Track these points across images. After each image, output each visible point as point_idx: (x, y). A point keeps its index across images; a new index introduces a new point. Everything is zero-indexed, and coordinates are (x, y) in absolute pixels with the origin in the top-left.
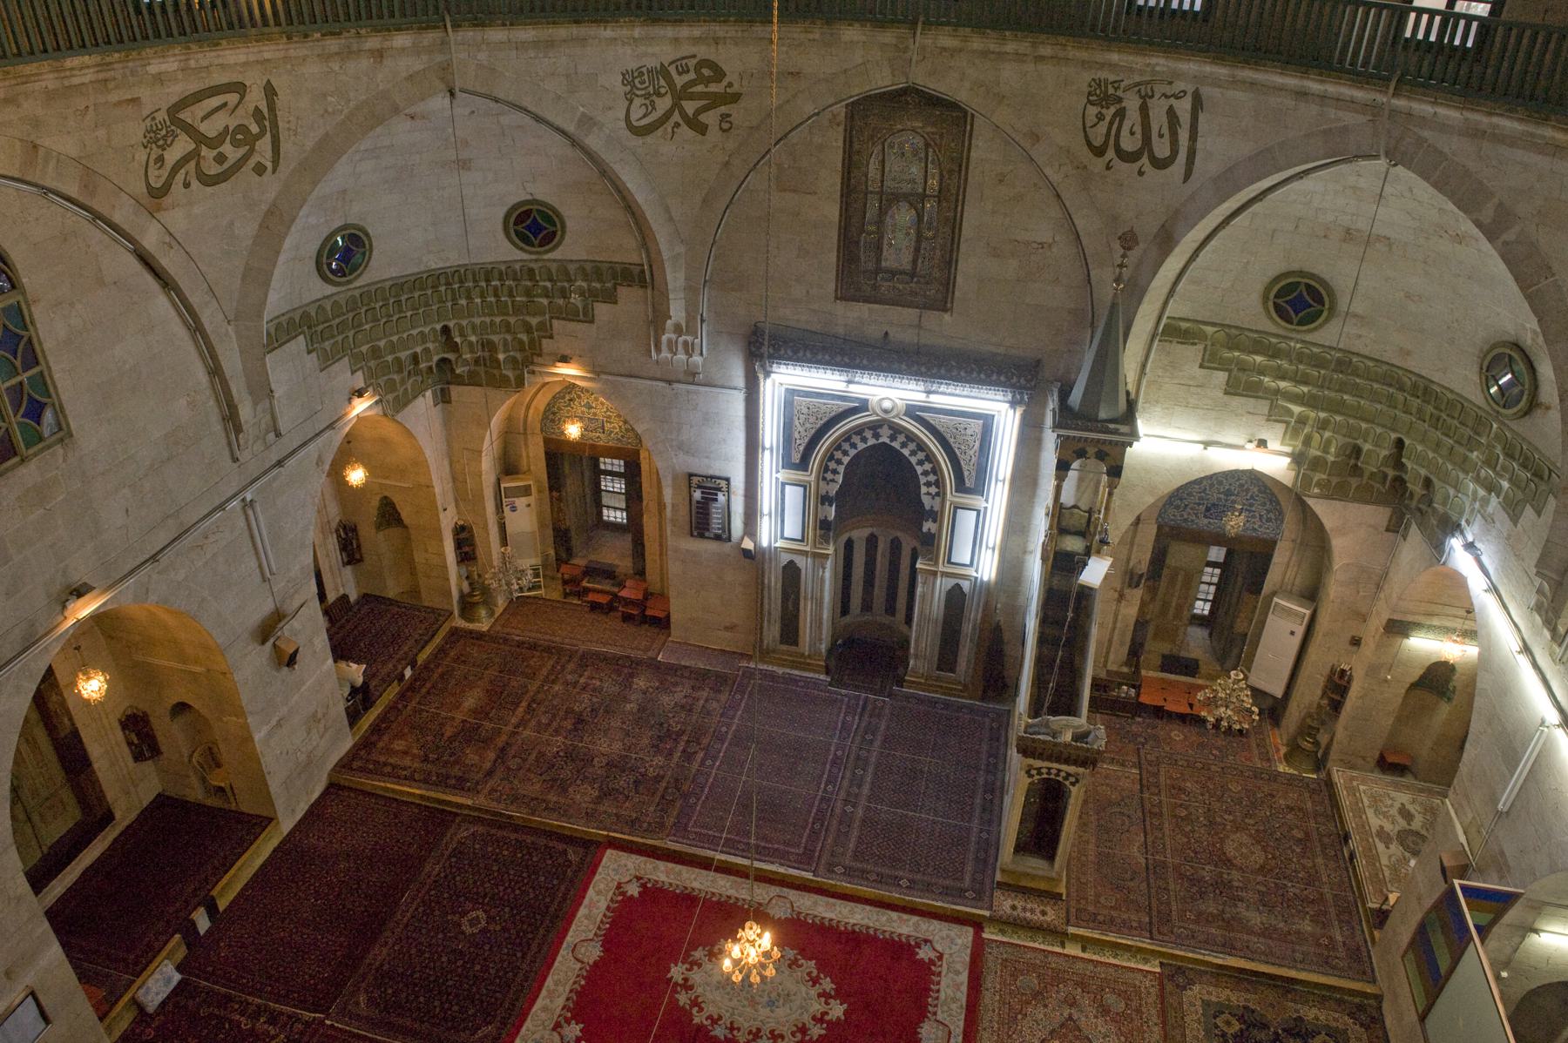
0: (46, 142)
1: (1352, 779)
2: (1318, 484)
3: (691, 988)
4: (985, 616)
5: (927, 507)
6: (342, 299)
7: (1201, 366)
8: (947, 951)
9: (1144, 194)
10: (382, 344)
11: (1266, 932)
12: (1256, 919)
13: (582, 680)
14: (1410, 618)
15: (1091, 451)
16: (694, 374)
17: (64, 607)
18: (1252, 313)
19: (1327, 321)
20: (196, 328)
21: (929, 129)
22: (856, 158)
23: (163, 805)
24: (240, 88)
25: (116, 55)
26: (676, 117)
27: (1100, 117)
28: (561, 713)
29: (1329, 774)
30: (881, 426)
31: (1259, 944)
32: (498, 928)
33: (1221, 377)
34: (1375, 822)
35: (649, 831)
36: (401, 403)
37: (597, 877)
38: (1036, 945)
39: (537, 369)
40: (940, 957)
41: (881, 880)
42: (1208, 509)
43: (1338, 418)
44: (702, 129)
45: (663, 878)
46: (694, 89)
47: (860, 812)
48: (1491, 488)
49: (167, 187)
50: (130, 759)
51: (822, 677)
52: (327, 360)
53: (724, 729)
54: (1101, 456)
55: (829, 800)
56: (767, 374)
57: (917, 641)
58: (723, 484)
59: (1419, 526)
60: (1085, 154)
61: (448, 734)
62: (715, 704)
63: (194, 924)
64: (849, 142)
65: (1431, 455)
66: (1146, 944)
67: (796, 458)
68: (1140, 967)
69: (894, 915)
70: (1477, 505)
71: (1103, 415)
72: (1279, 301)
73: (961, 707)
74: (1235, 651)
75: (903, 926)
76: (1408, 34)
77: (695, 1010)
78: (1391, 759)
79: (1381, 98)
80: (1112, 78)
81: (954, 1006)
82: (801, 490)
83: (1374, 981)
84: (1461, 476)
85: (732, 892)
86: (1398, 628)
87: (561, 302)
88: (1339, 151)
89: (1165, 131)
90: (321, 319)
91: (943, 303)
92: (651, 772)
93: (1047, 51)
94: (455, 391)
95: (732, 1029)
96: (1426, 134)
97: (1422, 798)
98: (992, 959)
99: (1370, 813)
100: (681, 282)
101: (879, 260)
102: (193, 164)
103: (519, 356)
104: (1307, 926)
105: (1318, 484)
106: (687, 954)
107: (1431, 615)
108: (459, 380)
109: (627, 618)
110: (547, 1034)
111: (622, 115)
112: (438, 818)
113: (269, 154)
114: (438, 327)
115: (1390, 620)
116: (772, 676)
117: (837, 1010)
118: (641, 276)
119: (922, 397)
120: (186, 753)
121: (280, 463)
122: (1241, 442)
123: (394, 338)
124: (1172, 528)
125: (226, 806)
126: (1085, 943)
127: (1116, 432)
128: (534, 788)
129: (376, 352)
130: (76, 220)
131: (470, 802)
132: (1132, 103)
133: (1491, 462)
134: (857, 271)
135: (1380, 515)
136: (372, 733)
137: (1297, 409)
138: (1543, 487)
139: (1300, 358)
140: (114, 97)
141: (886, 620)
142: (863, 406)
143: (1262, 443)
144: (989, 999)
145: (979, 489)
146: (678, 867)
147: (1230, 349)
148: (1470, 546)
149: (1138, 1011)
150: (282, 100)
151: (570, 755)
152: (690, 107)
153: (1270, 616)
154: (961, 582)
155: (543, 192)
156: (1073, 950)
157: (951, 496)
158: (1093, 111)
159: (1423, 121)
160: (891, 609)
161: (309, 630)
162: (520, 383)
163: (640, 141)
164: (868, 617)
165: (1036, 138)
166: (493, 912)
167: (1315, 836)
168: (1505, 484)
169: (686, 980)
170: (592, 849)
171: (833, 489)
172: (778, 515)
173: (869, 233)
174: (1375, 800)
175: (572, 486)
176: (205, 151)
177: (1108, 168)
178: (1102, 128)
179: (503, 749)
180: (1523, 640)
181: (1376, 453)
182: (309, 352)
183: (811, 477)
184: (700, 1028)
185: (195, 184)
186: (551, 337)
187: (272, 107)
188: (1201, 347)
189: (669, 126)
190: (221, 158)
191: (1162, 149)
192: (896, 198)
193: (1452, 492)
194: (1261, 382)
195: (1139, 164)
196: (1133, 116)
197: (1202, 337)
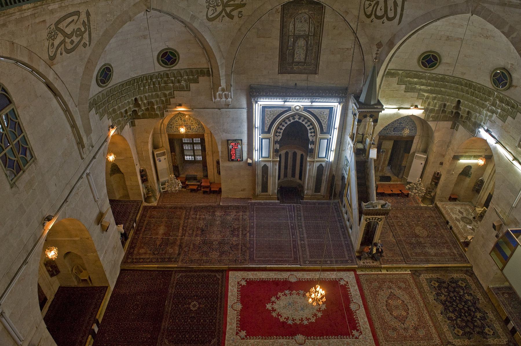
0: (16, 41)
1: (443, 205)
2: (432, 117)
3: (275, 310)
4: (330, 173)
5: (311, 140)
6: (105, 92)
8: (349, 281)
9: (384, 30)
10: (116, 107)
11: (436, 255)
12: (432, 251)
13: (198, 216)
14: (460, 154)
15: (369, 115)
16: (228, 105)
17: (44, 226)
18: (414, 65)
20: (67, 111)
21: (310, 12)
22: (285, 24)
23: (62, 289)
24: (77, 13)
25: (39, 3)
26: (224, 13)
28: (195, 229)
29: (436, 204)
30: (295, 115)
31: (435, 258)
32: (203, 306)
33: (404, 86)
34: (454, 216)
35: (241, 263)
36: (122, 128)
37: (230, 282)
39: (169, 110)
40: (347, 283)
42: (394, 129)
43: (439, 96)
44: (231, 17)
46: (230, 3)
47: (306, 243)
48: (493, 112)
49: (55, 55)
50: (49, 277)
51: (277, 201)
52: (101, 116)
53: (252, 224)
54: (371, 116)
55: (295, 241)
56: (256, 102)
59: (463, 126)
60: (363, 17)
61: (158, 244)
62: (246, 217)
63: (94, 330)
64: (282, 18)
65: (470, 104)
66: (405, 265)
67: (266, 129)
69: (329, 273)
70: (487, 118)
71: (372, 103)
72: (423, 61)
73: (323, 203)
74: (402, 172)
77: (279, 317)
78: (452, 197)
81: (357, 297)
82: (268, 140)
84: (482, 110)
85: (275, 277)
86: (456, 158)
87: (178, 84)
89: (393, 8)
90: (99, 101)
92: (235, 243)
94: (137, 121)
95: (293, 320)
97: (463, 207)
98: (362, 280)
99: (451, 214)
100: (224, 73)
101: (293, 60)
102: (63, 45)
103: (161, 106)
105: (432, 117)
106: (270, 299)
108: (139, 118)
109: (205, 192)
111: (205, 14)
112: (166, 274)
113: (88, 39)
114: (134, 99)
115: (454, 156)
116: (261, 204)
117: (269, 306)
118: (207, 73)
119: (310, 104)
120: (70, 269)
121: (94, 157)
123: (120, 105)
124: (383, 136)
125: (87, 286)
126: (387, 269)
127: (377, 108)
128: (197, 256)
129: (114, 111)
130: (26, 72)
131: (176, 266)
133: (494, 104)
134: (286, 63)
135: (449, 124)
136: (130, 248)
137: (426, 94)
138: (514, 110)
139: (429, 78)
140: (37, 20)
141: (292, 179)
142: (289, 109)
143: (416, 107)
144: (366, 292)
145: (329, 132)
146: (255, 272)
147: (407, 77)
148: (487, 131)
149: (409, 286)
150: (92, 18)
151: (204, 242)
152: (228, 9)
153: (414, 159)
154: (322, 163)
155: (171, 45)
156: (384, 272)
157: (319, 136)
158: (367, 3)
160: (293, 175)
161: (109, 218)
162: (163, 115)
163: (211, 23)
164: (286, 179)
165: (347, 13)
166: (199, 301)
167: (438, 223)
168: (499, 111)
169: (272, 308)
170: (225, 272)
172: (260, 150)
173: (290, 50)
174: (451, 209)
175: (177, 149)
176: (68, 40)
177: (383, 23)
178: (371, 8)
179: (180, 245)
180: (513, 156)
181: (451, 105)
182: (96, 114)
183: (272, 135)
184: (283, 323)
185: (64, 53)
186: (174, 98)
187: (89, 21)
188: (397, 78)
189: (221, 17)
190: (72, 42)
191: (391, 14)
192: (299, 37)
193: (478, 115)
195: (382, 20)
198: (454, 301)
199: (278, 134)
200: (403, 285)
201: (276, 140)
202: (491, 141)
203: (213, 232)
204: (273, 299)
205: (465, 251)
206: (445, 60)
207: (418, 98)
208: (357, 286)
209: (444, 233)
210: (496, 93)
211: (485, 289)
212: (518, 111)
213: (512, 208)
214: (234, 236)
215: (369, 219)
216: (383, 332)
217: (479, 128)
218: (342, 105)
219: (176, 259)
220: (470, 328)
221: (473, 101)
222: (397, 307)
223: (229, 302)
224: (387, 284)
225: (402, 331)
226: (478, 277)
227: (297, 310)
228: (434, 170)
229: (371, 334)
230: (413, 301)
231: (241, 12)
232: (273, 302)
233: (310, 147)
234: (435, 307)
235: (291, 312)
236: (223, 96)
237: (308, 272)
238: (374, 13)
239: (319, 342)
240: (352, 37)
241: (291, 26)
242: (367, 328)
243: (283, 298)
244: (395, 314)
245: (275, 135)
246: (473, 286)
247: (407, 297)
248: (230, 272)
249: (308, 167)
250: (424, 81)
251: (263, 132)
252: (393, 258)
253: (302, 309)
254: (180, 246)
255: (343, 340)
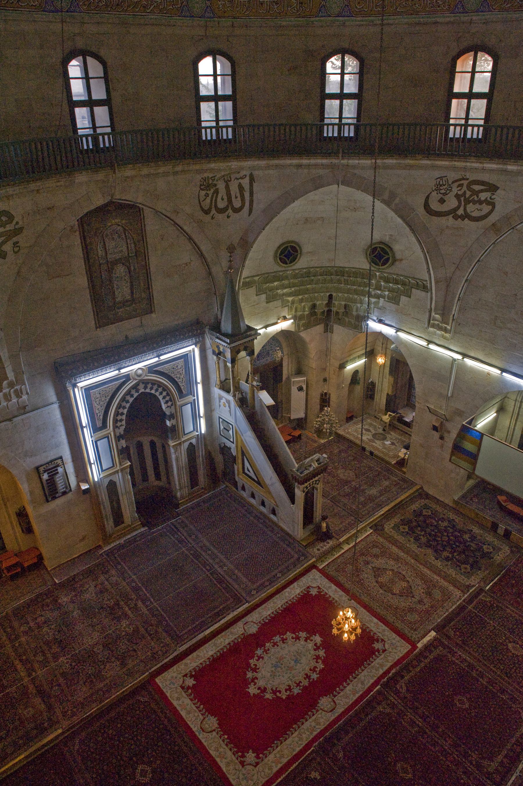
3: (265, 689)
5: (168, 413)
7: (257, 295)
8: (319, 584)
9: (232, 226)
12: (374, 491)
14: (345, 360)
15: (242, 348)
16: (25, 407)
18: (271, 265)
19: (300, 257)
21: (124, 222)
27: (207, 195)
28: (45, 647)
37: (168, 695)
38: (336, 556)
40: (319, 588)
41: (271, 582)
43: (306, 296)
45: (194, 665)
46: (482, 187)
48: (378, 297)
51: (143, 529)
54: (245, 349)
56: (75, 386)
57: (179, 481)
58: (59, 461)
60: (200, 215)
62: (114, 579)
64: (84, 238)
65: (346, 295)
67: (99, 424)
68: (367, 534)
69: (288, 589)
73: (210, 498)
75: (294, 591)
76: (204, 138)
79: (335, 161)
80: (211, 175)
83: (416, 484)
84: (362, 298)
85: (227, 642)
86: (342, 366)
88: (317, 184)
89: (238, 195)
91: (150, 310)
92: (130, 630)
93: (179, 168)
95: (298, 685)
96: (356, 171)
100: (7, 355)
104: (386, 483)
107: (350, 356)
109: (13, 578)
110: (244, 771)
116: (121, 547)
119: (156, 359)
122: (275, 321)
126: (347, 542)
131: (60, 731)
132: (221, 186)
134: (104, 309)
135: (320, 328)
137: (290, 299)
141: (146, 484)
142: (128, 377)
145: (191, 392)
148: (380, 321)
158: (203, 193)
159: (354, 167)
160: (145, 478)
168: (387, 293)
169: (259, 688)
171: (121, 430)
177: (213, 218)
178: (208, 200)
184: (288, 697)
188: (254, 287)
191: (237, 204)
192: (116, 262)
193: (359, 305)
194: (277, 293)
195: (227, 213)
196: (222, 192)
197: (255, 282)
198: (435, 536)
199: (119, 424)
200: (376, 551)
201: (118, 434)
202: (388, 331)
203: (80, 634)
204: (250, 675)
205: (404, 473)
206: (305, 249)
207: (283, 306)
208: (333, 585)
209: (368, 463)
210: (378, 274)
211: (451, 504)
212: (412, 288)
213: (448, 398)
214: (119, 619)
215: (307, 487)
216: (403, 621)
217: (368, 320)
218: (199, 345)
219: (50, 719)
220: (472, 557)
221: (349, 291)
222: (392, 581)
223: (192, 726)
224: (361, 559)
225: (419, 607)
226: (435, 496)
227: (291, 669)
228: (320, 391)
229: (394, 635)
230: (402, 564)
231: (17, 242)
232: (254, 679)
233: (168, 423)
234: (425, 555)
235: (286, 676)
236: (13, 395)
237: (263, 606)
238: (213, 206)
239: (350, 691)
240: (189, 246)
241: (101, 253)
242: (384, 631)
243: (260, 664)
244: (396, 591)
245: (115, 427)
246: (439, 509)
247: (392, 563)
248: (157, 680)
249: (173, 456)
250: (286, 282)
251: (95, 429)
252: (344, 524)
253: (297, 661)
254: (41, 692)
255: (372, 664)
